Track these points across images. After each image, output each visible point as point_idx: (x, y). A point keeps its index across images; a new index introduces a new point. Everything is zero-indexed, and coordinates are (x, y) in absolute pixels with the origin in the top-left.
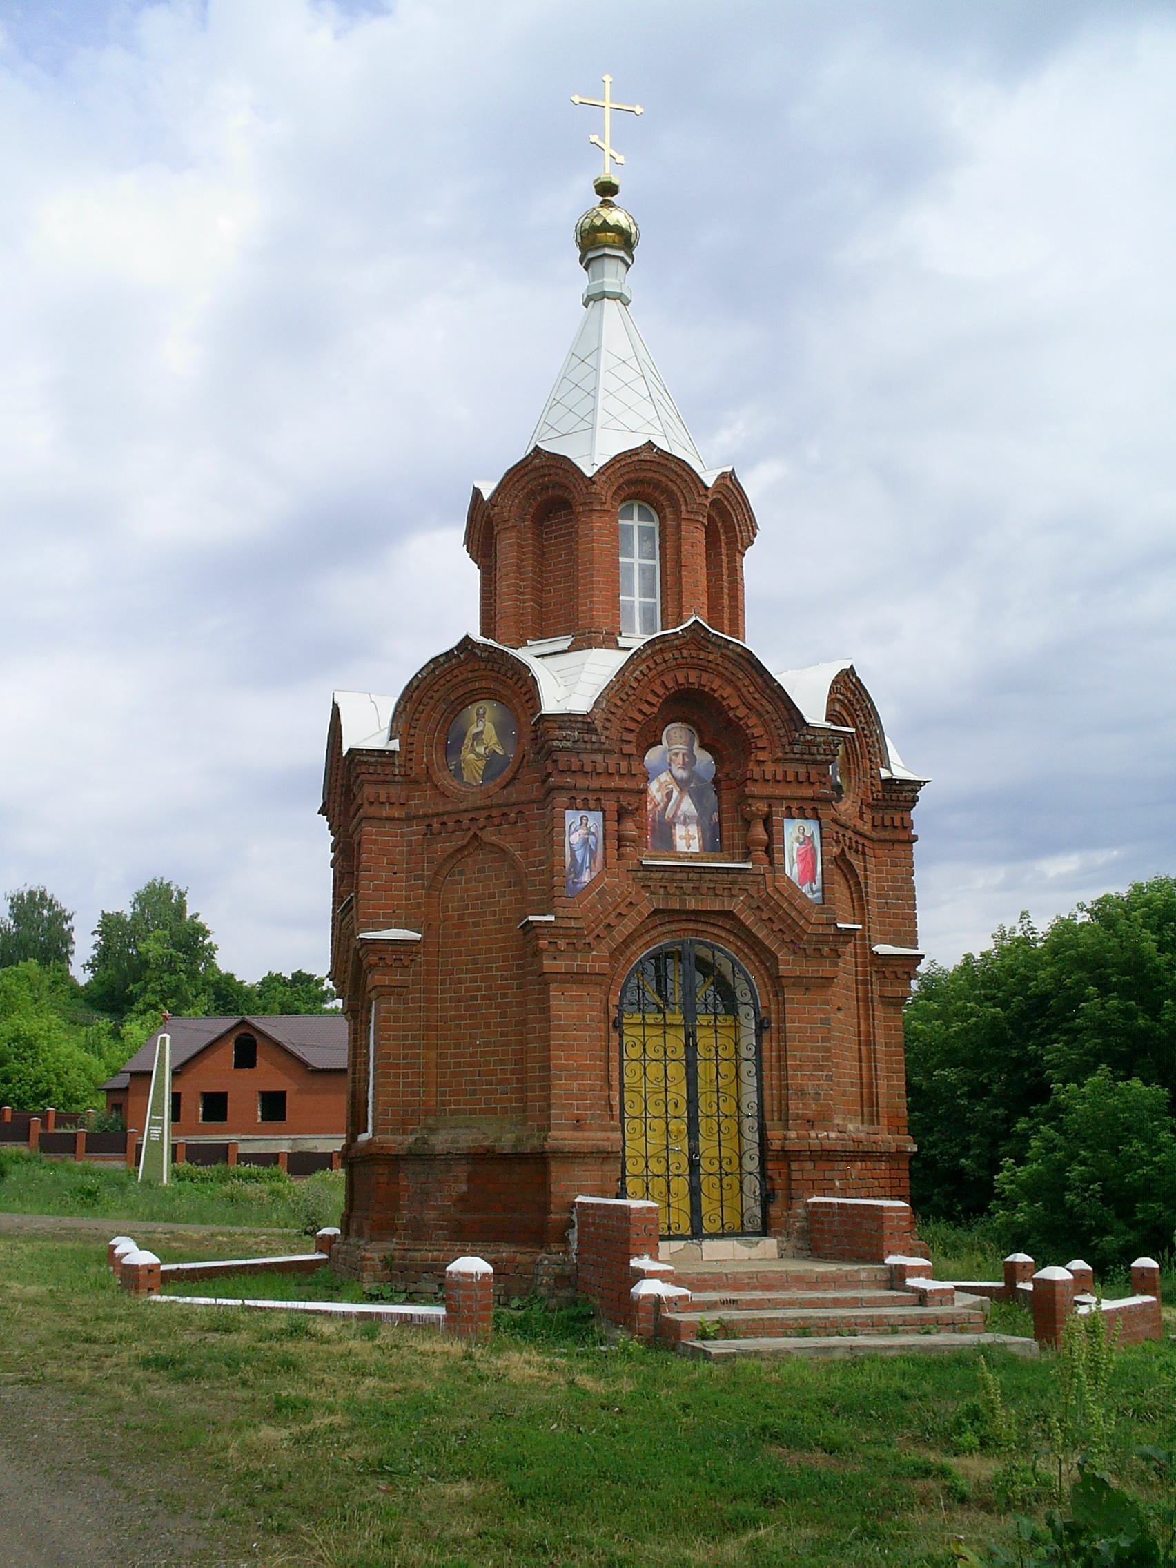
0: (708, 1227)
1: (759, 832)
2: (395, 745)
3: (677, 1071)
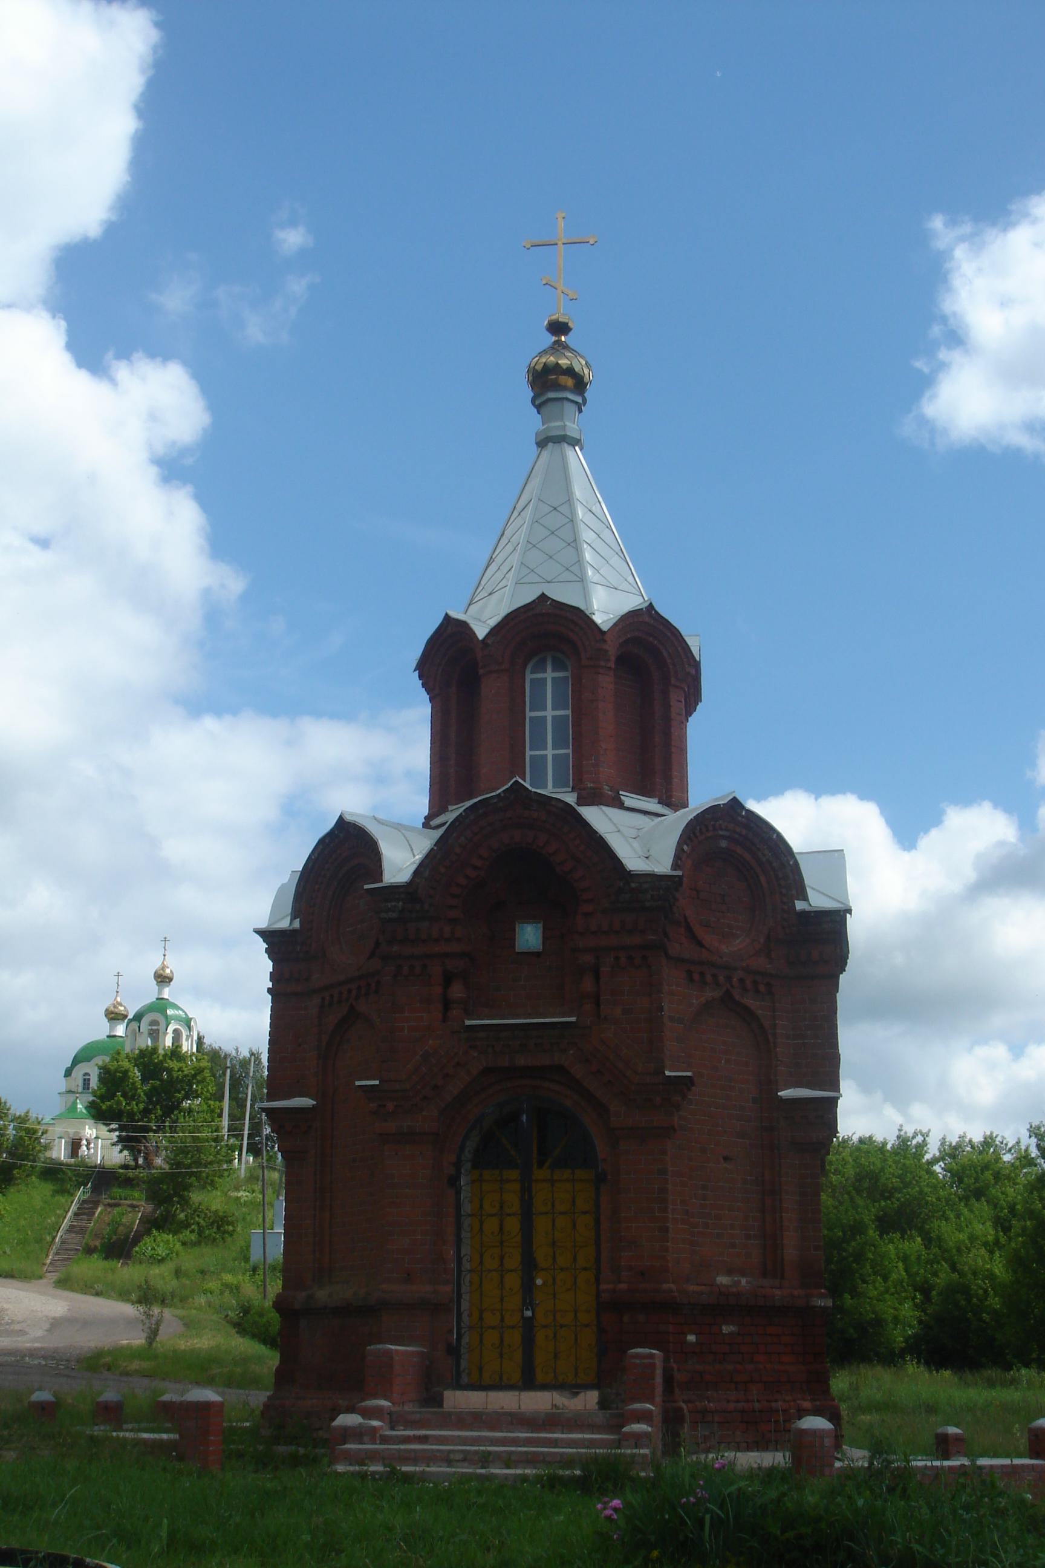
0: (540, 1377)
1: (588, 984)
2: (297, 924)
3: (513, 1225)
